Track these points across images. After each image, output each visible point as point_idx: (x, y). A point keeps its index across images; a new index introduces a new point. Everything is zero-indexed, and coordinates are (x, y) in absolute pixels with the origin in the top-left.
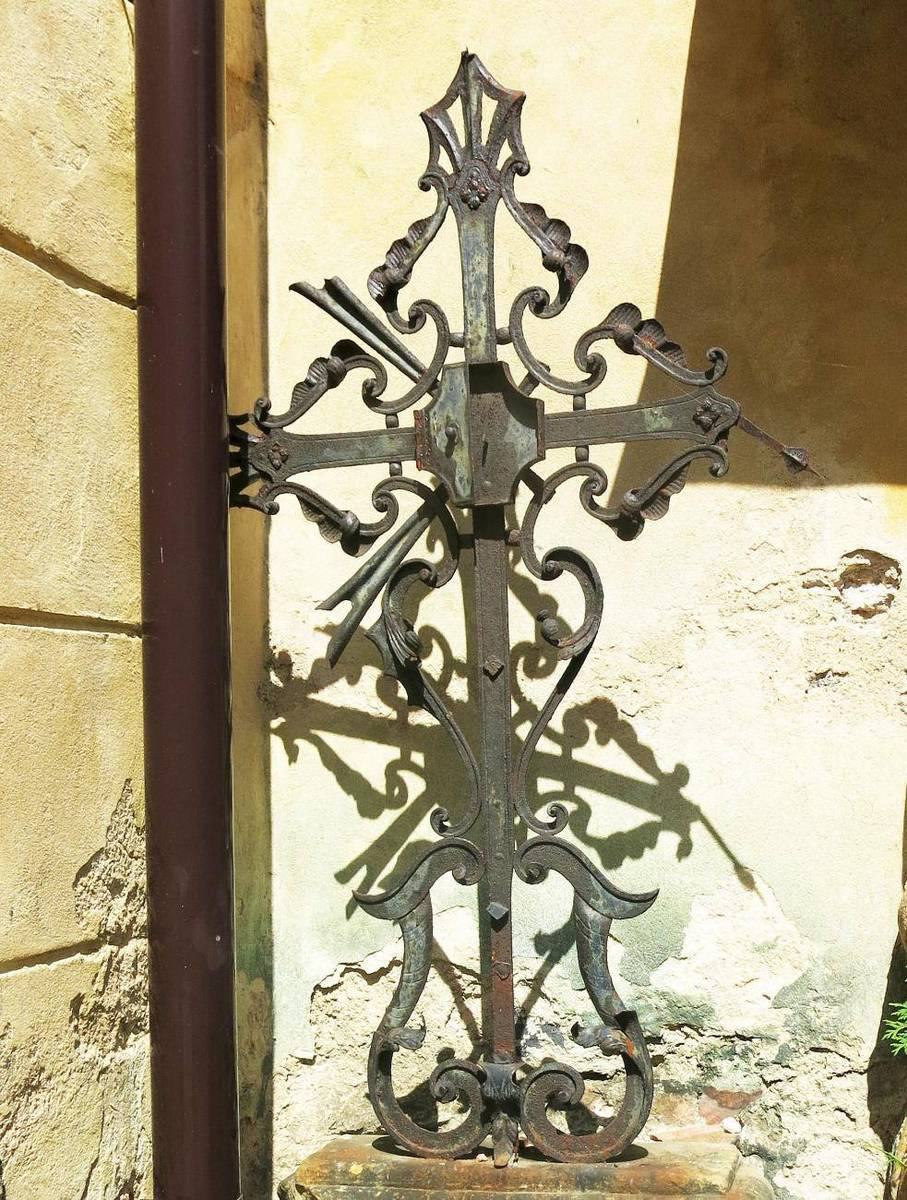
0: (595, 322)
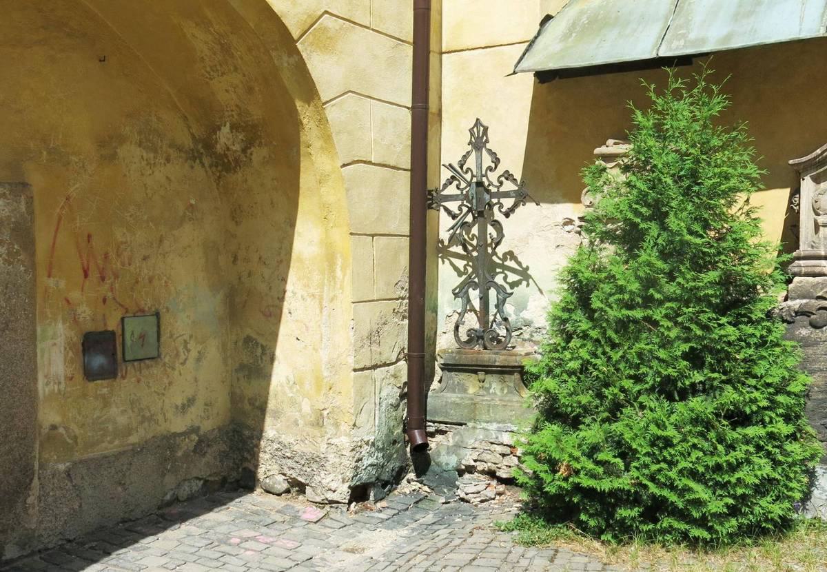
0: (501, 173)
